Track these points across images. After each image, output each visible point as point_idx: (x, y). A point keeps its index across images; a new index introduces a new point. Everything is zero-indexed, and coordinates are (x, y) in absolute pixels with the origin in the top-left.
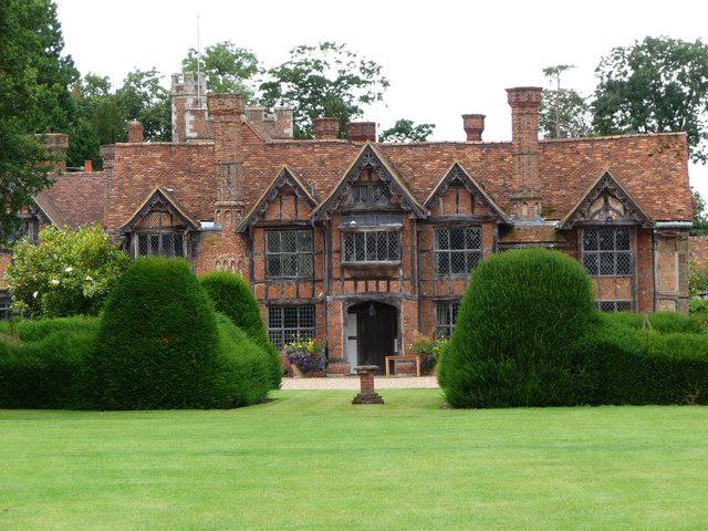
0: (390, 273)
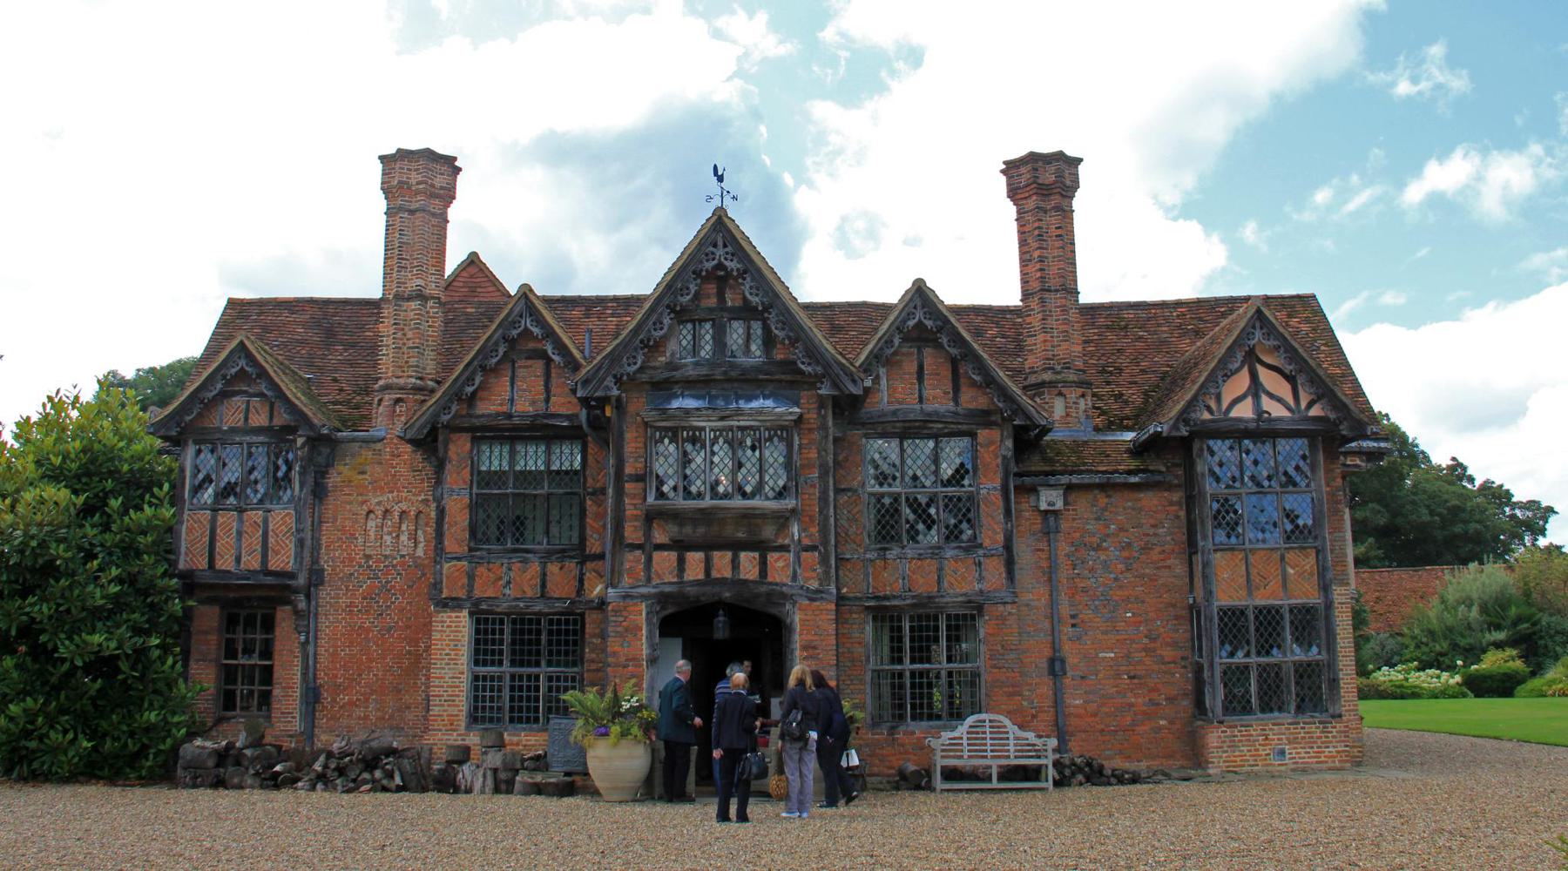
0: (768, 532)
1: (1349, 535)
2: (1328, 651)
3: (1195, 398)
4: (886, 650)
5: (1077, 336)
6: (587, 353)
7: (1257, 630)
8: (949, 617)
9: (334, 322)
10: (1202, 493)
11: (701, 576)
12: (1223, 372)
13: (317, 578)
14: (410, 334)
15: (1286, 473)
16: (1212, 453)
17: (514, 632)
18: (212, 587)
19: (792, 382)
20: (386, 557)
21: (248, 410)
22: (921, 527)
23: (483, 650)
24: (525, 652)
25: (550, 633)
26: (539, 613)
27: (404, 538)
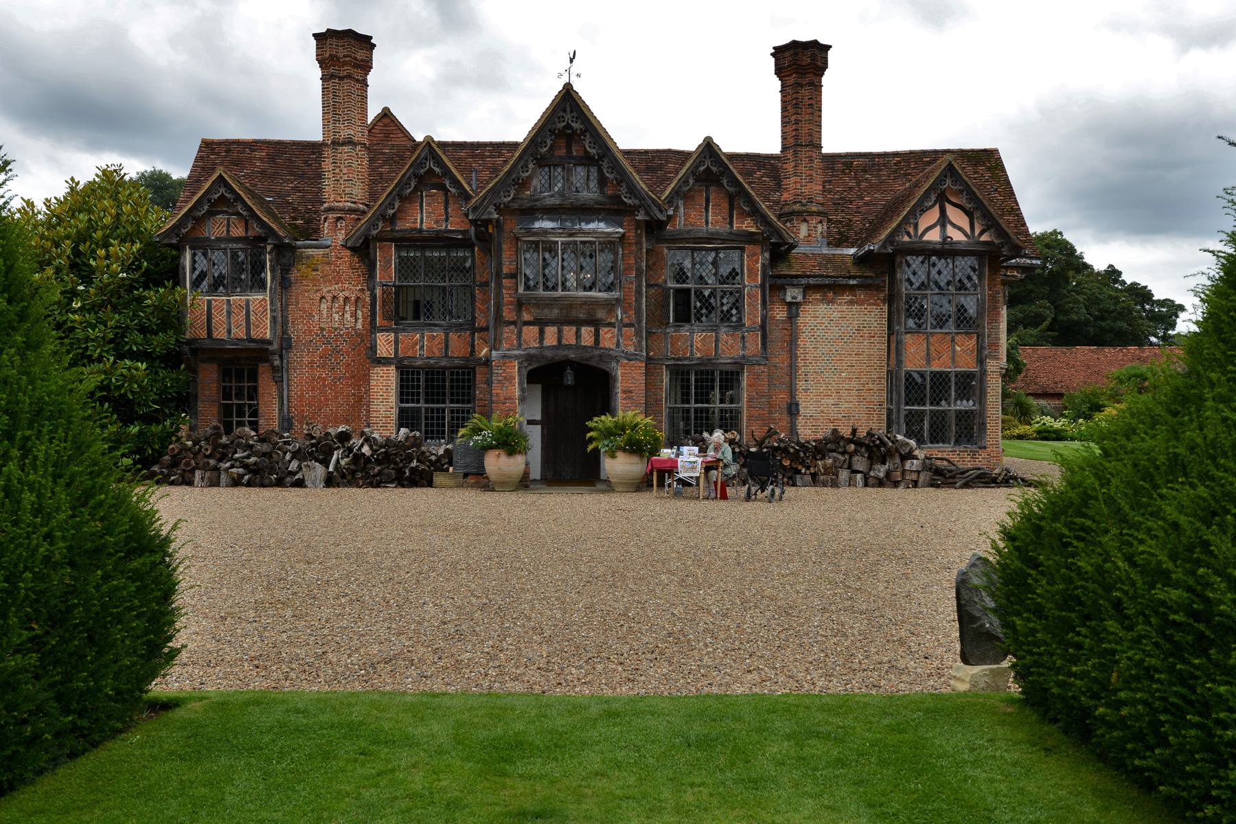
0: (601, 314)
1: (1003, 326)
2: (980, 403)
3: (899, 225)
4: (679, 394)
5: (819, 178)
6: (474, 187)
7: (931, 388)
8: (721, 373)
9: (292, 160)
10: (899, 294)
11: (555, 343)
12: (920, 209)
13: (286, 344)
14: (345, 171)
15: (960, 281)
16: (909, 265)
17: (427, 380)
18: (211, 350)
19: (616, 211)
20: (336, 329)
21: (228, 225)
22: (704, 311)
23: (405, 391)
24: (434, 395)
25: (452, 380)
26: (445, 368)
27: (348, 316)
